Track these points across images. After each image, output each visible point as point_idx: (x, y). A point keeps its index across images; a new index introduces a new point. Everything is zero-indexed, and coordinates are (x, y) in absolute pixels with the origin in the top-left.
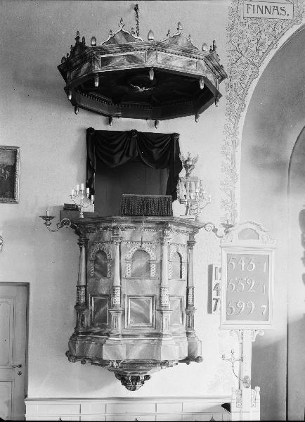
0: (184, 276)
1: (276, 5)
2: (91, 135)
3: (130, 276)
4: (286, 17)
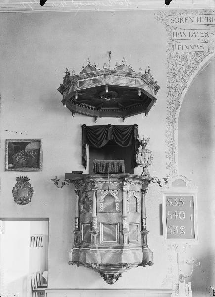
0: (139, 211)
2: (86, 130)
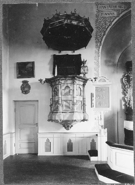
1: (111, 12)
2: (54, 55)
3: (64, 94)
4: (114, 15)
